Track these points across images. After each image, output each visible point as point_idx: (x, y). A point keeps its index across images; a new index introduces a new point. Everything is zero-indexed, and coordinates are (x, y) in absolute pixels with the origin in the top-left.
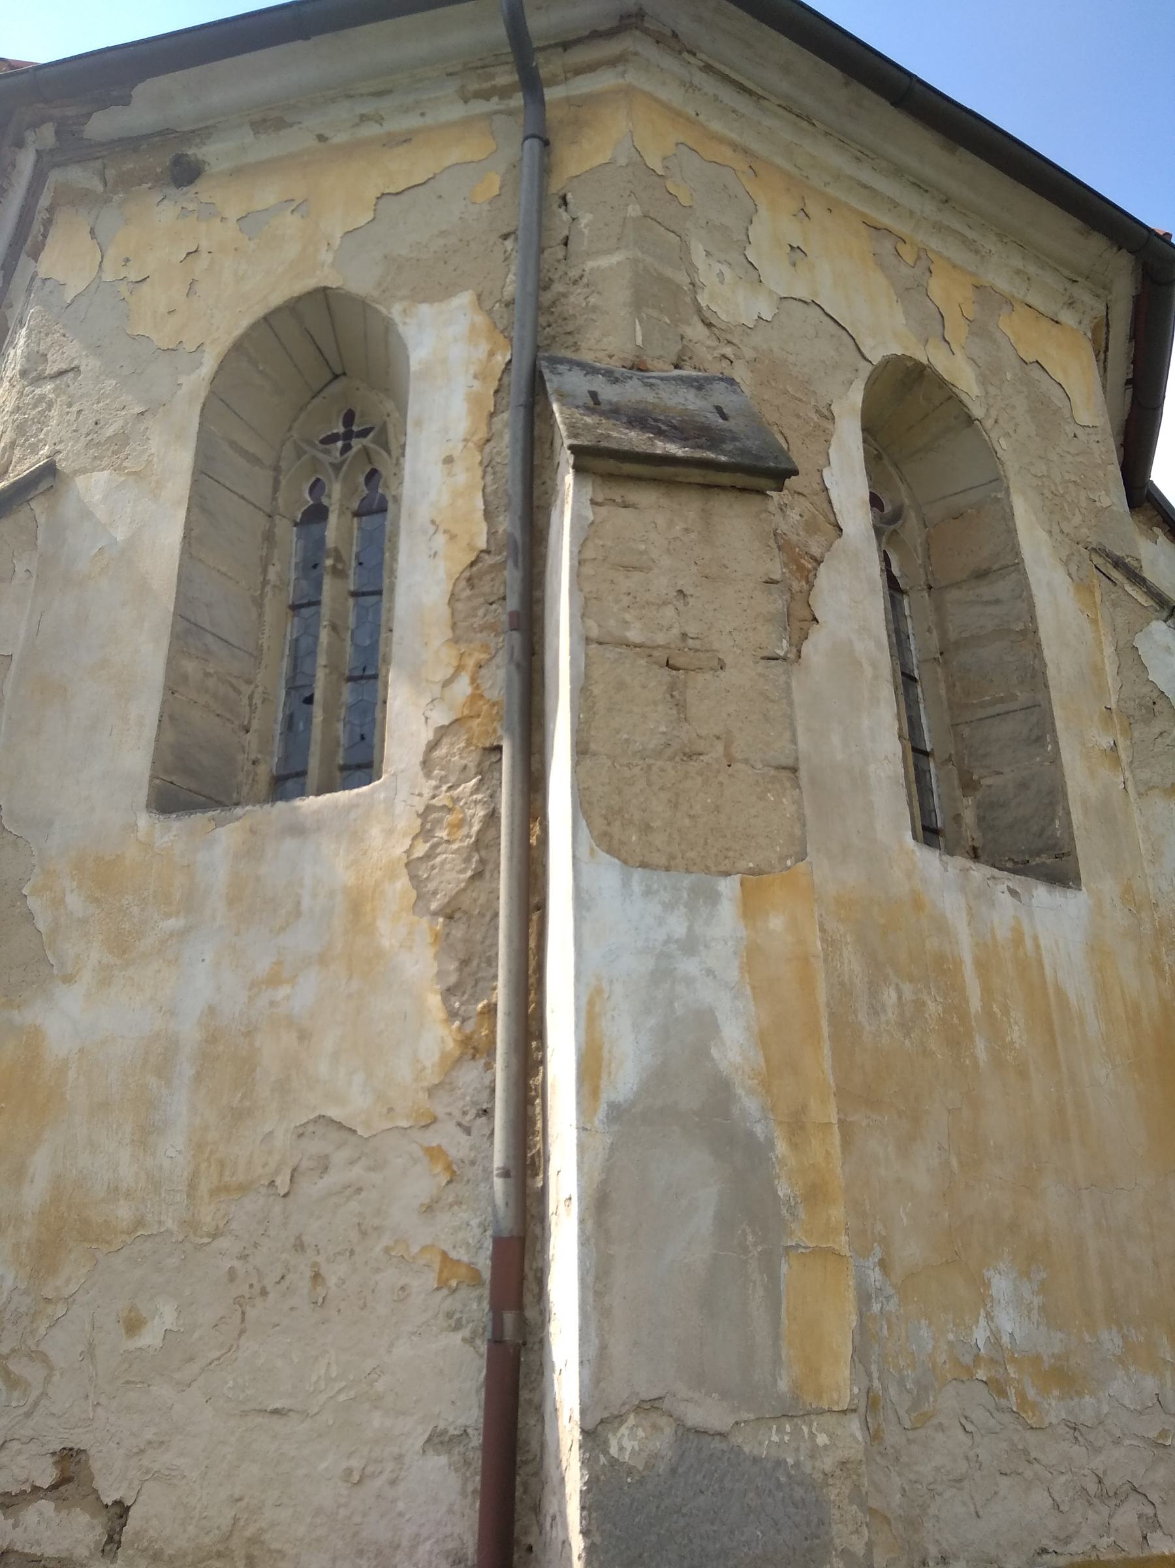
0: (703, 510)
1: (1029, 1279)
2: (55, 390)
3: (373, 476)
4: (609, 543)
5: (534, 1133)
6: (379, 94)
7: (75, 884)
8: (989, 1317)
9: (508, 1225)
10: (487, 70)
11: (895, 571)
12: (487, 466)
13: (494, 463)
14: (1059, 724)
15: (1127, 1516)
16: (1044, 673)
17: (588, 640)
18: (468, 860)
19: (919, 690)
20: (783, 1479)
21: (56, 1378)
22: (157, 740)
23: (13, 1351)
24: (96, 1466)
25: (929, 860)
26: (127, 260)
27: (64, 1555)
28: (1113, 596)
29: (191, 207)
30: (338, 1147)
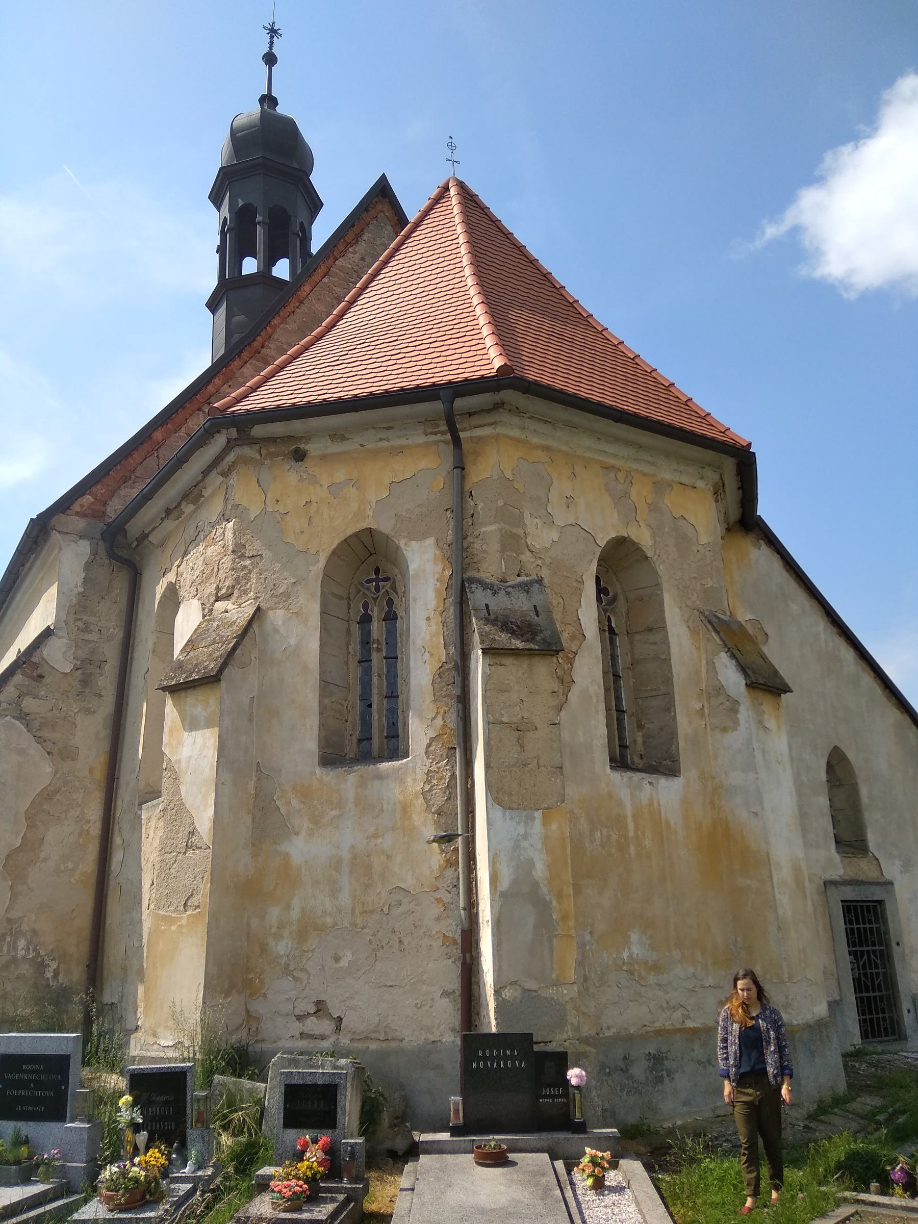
1: (646, 935)
3: (390, 603)
5: (473, 894)
6: (388, 428)
8: (629, 948)
9: (466, 927)
10: (436, 422)
11: (613, 625)
12: (444, 623)
13: (446, 621)
14: (677, 703)
15: (678, 1015)
16: (672, 679)
17: (489, 723)
18: (445, 793)
19: (622, 682)
20: (554, 1004)
21: (312, 978)
22: (319, 736)
23: (295, 969)
25: (618, 778)
26: (278, 501)
27: (322, 1034)
28: (708, 636)
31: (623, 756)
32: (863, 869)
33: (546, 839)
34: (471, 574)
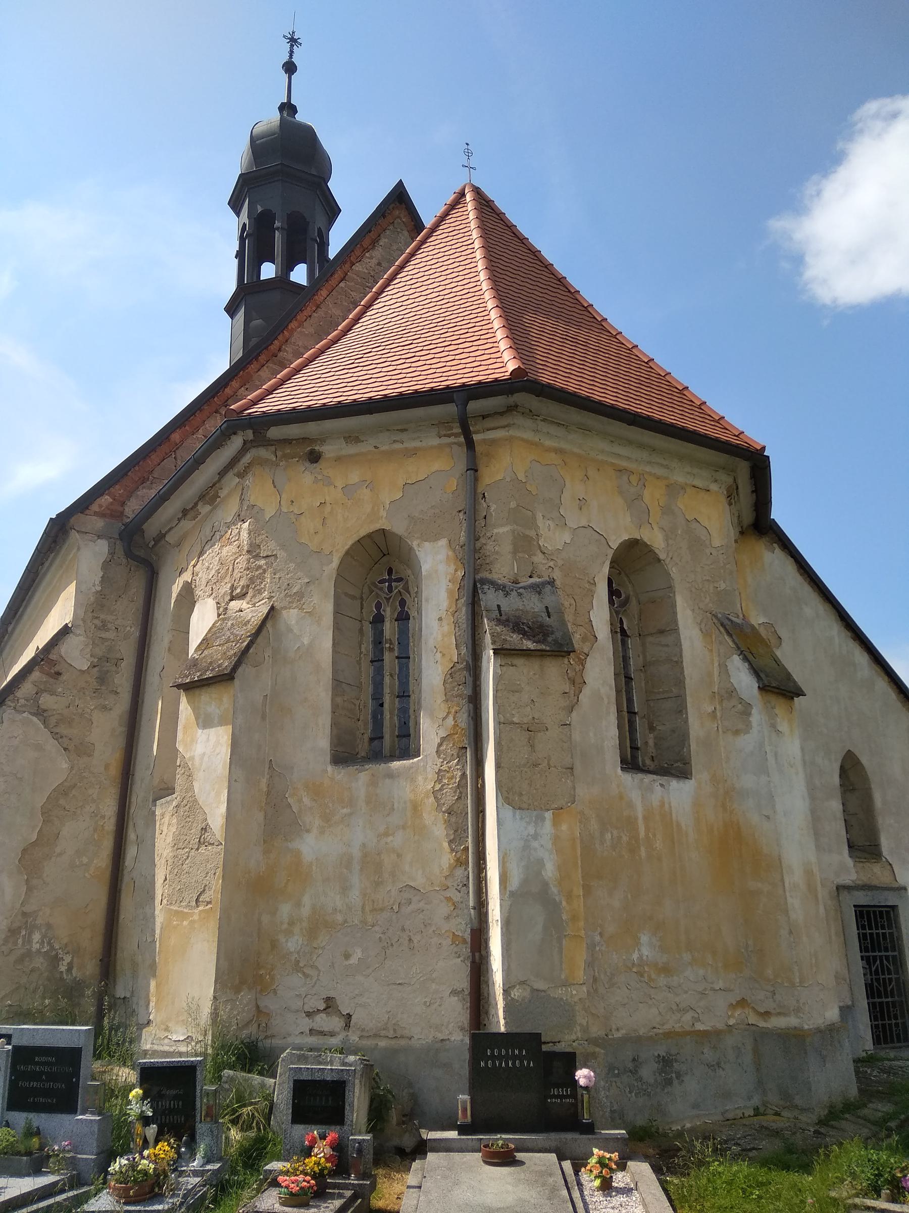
0: (540, 665)
2: (266, 564)
3: (403, 603)
4: (507, 682)
7: (306, 793)
8: (639, 950)
9: (476, 926)
11: (625, 627)
12: (456, 623)
14: (689, 705)
15: (688, 1017)
17: (500, 723)
20: (562, 1004)
24: (339, 1003)
25: (629, 779)
26: (293, 502)
27: (331, 1030)
29: (320, 477)
30: (414, 896)
31: (634, 757)
32: (876, 874)
33: (556, 839)
34: (484, 575)
